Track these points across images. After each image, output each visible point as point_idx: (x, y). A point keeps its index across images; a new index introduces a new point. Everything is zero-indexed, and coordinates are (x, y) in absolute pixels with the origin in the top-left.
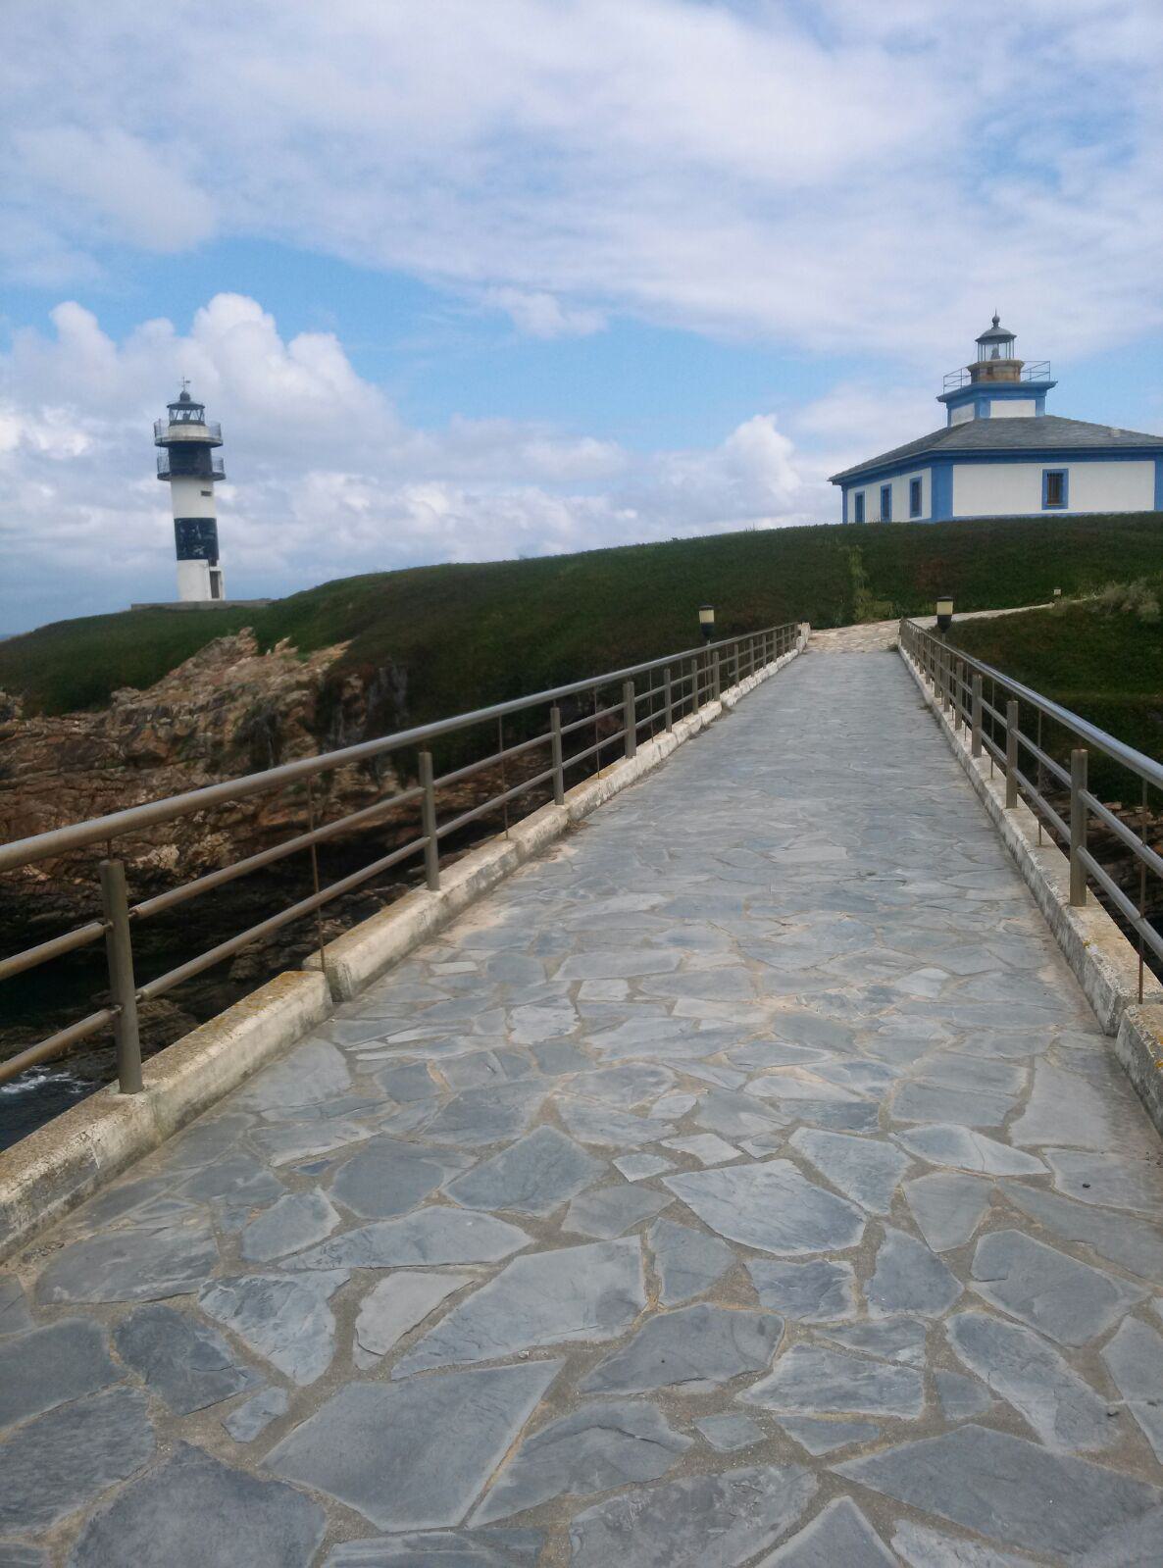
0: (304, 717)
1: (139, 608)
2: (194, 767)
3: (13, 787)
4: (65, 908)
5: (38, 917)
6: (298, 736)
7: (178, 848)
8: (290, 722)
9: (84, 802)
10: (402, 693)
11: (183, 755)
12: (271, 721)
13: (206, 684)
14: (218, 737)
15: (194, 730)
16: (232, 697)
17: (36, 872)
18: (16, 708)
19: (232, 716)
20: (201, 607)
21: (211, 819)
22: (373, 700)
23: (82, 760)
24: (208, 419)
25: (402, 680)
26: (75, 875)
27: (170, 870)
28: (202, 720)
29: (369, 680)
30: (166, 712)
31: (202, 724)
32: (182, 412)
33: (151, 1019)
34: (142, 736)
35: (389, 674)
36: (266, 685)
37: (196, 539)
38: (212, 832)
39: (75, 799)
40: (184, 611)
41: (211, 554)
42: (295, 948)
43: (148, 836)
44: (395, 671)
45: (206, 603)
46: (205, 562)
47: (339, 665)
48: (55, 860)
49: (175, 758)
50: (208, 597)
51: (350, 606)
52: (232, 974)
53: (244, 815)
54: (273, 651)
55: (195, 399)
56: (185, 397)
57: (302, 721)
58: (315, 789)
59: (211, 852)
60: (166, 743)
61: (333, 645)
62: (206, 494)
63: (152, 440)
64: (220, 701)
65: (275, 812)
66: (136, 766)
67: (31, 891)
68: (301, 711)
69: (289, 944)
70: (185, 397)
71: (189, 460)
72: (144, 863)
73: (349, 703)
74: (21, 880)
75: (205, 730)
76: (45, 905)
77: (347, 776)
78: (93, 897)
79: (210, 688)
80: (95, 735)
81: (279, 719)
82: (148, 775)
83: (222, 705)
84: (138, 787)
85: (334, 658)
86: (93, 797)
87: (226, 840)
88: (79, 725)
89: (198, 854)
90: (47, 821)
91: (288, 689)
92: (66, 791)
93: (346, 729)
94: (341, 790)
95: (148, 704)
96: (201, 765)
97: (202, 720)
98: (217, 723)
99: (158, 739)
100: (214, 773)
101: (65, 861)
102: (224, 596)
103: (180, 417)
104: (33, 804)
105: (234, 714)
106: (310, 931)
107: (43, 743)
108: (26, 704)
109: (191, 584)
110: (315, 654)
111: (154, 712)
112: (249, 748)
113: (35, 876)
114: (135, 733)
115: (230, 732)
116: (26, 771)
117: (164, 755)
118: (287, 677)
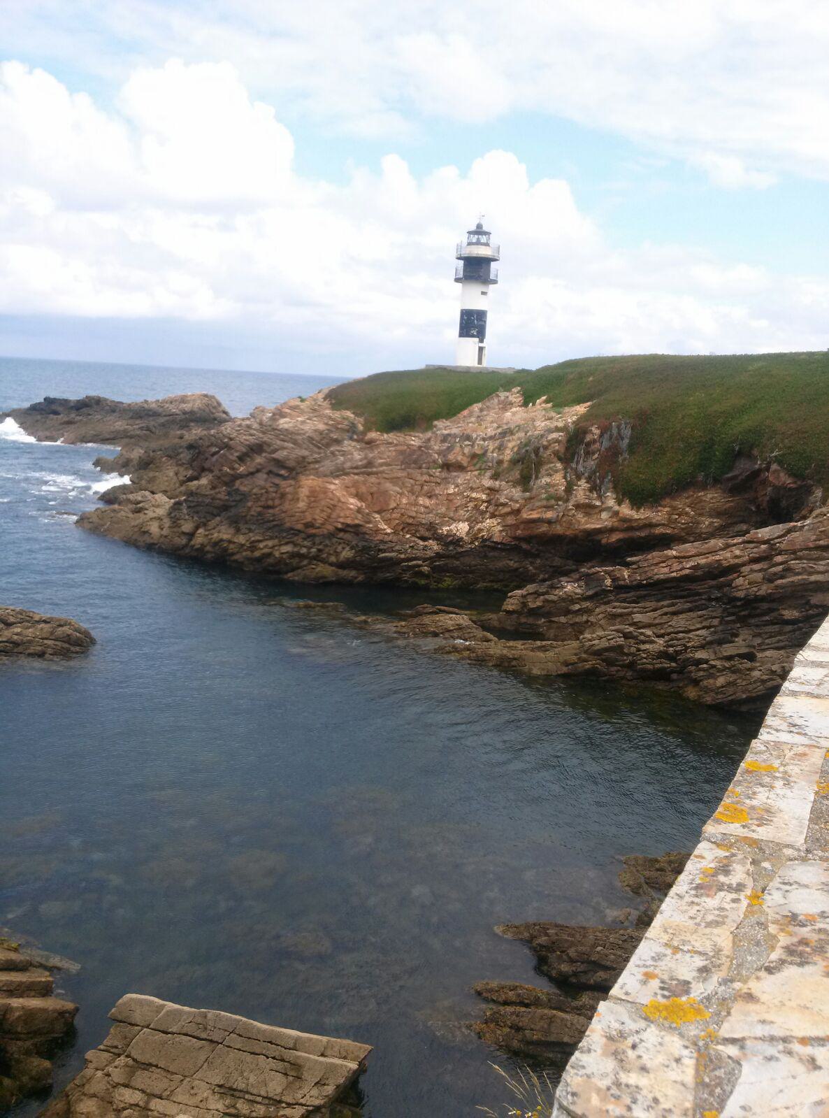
0: (558, 451)
1: (431, 368)
2: (484, 475)
3: (376, 473)
4: (399, 552)
5: (383, 555)
6: (552, 463)
8: (548, 452)
9: (417, 488)
10: (626, 441)
11: (478, 466)
12: (537, 451)
13: (492, 422)
14: (501, 457)
15: (486, 451)
16: (511, 432)
17: (386, 527)
18: (360, 425)
19: (510, 445)
20: (472, 370)
21: (491, 509)
22: (606, 444)
23: (415, 462)
24: (494, 240)
25: (627, 432)
26: (407, 533)
28: (491, 446)
29: (604, 430)
30: (468, 438)
31: (491, 448)
32: (476, 236)
33: (457, 625)
34: (455, 451)
35: (618, 427)
36: (534, 427)
37: (472, 324)
38: (491, 518)
39: (412, 485)
40: (460, 372)
41: (481, 335)
42: (546, 597)
43: (452, 515)
44: (623, 426)
45: (473, 367)
46: (477, 340)
47: (583, 418)
48: (397, 521)
49: (472, 468)
51: (591, 379)
52: (504, 607)
54: (534, 405)
55: (485, 228)
56: (479, 226)
57: (556, 454)
58: (558, 499)
59: (488, 531)
60: (468, 457)
61: (579, 404)
62: (483, 293)
63: (455, 255)
64: (504, 434)
65: (532, 510)
66: (448, 469)
67: (381, 538)
68: (556, 446)
69: (543, 594)
70: (479, 226)
71: (476, 269)
72: (448, 531)
73: (588, 444)
75: (492, 452)
76: (388, 548)
77: (582, 493)
78: (415, 547)
79: (495, 425)
80: (425, 447)
81: (541, 450)
82: (456, 476)
83: (503, 437)
84: (449, 483)
85: (580, 413)
86: (422, 486)
87: (498, 524)
88: (414, 440)
89: (480, 530)
91: (550, 431)
92: (407, 480)
93: (584, 461)
94: (576, 501)
95: (455, 431)
96: (488, 474)
97: (491, 446)
98: (500, 448)
99: (464, 454)
100: (496, 479)
101: (403, 523)
102: (485, 364)
103: (474, 240)
104: (388, 485)
105: (512, 444)
106: (558, 588)
107: (393, 449)
108: (366, 423)
109: (464, 354)
110: (567, 409)
111: (461, 437)
112: (519, 466)
113: (385, 530)
114: (450, 449)
115: (508, 455)
116: (381, 465)
117: (465, 464)
118: (548, 423)
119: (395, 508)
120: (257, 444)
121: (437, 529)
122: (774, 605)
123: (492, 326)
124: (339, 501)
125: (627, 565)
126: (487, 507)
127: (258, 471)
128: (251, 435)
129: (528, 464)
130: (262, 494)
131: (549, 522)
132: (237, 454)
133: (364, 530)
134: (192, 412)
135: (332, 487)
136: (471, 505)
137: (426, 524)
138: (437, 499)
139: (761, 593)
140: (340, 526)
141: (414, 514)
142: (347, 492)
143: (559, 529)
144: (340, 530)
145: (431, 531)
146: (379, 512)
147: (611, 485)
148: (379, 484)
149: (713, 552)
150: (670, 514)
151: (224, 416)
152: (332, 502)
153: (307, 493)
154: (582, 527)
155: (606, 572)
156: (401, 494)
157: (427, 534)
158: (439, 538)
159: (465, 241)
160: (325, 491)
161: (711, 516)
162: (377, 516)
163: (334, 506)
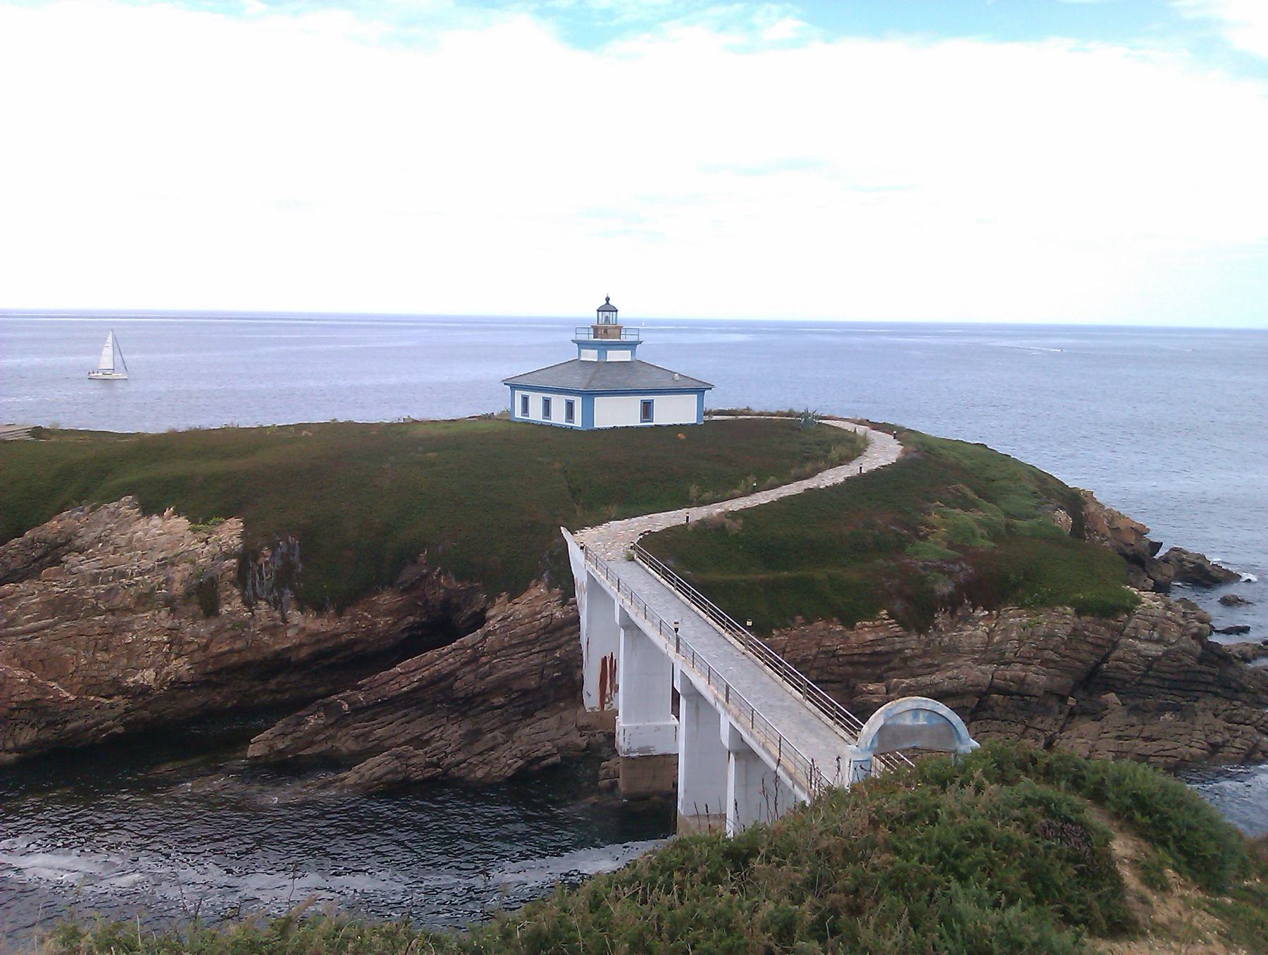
43: (134, 665)
49: (142, 609)
105: (180, 573)
122: (486, 697)
125: (359, 688)
126: (170, 649)
129: (204, 595)
131: (239, 651)
133: (45, 703)
136: (152, 649)
139: (477, 690)
140: (14, 705)
141: (95, 674)
142: (11, 664)
143: (250, 656)
145: (117, 687)
147: (293, 604)
149: (431, 663)
150: (352, 621)
154: (271, 649)
155: (342, 698)
157: (112, 691)
158: (125, 692)
161: (385, 616)
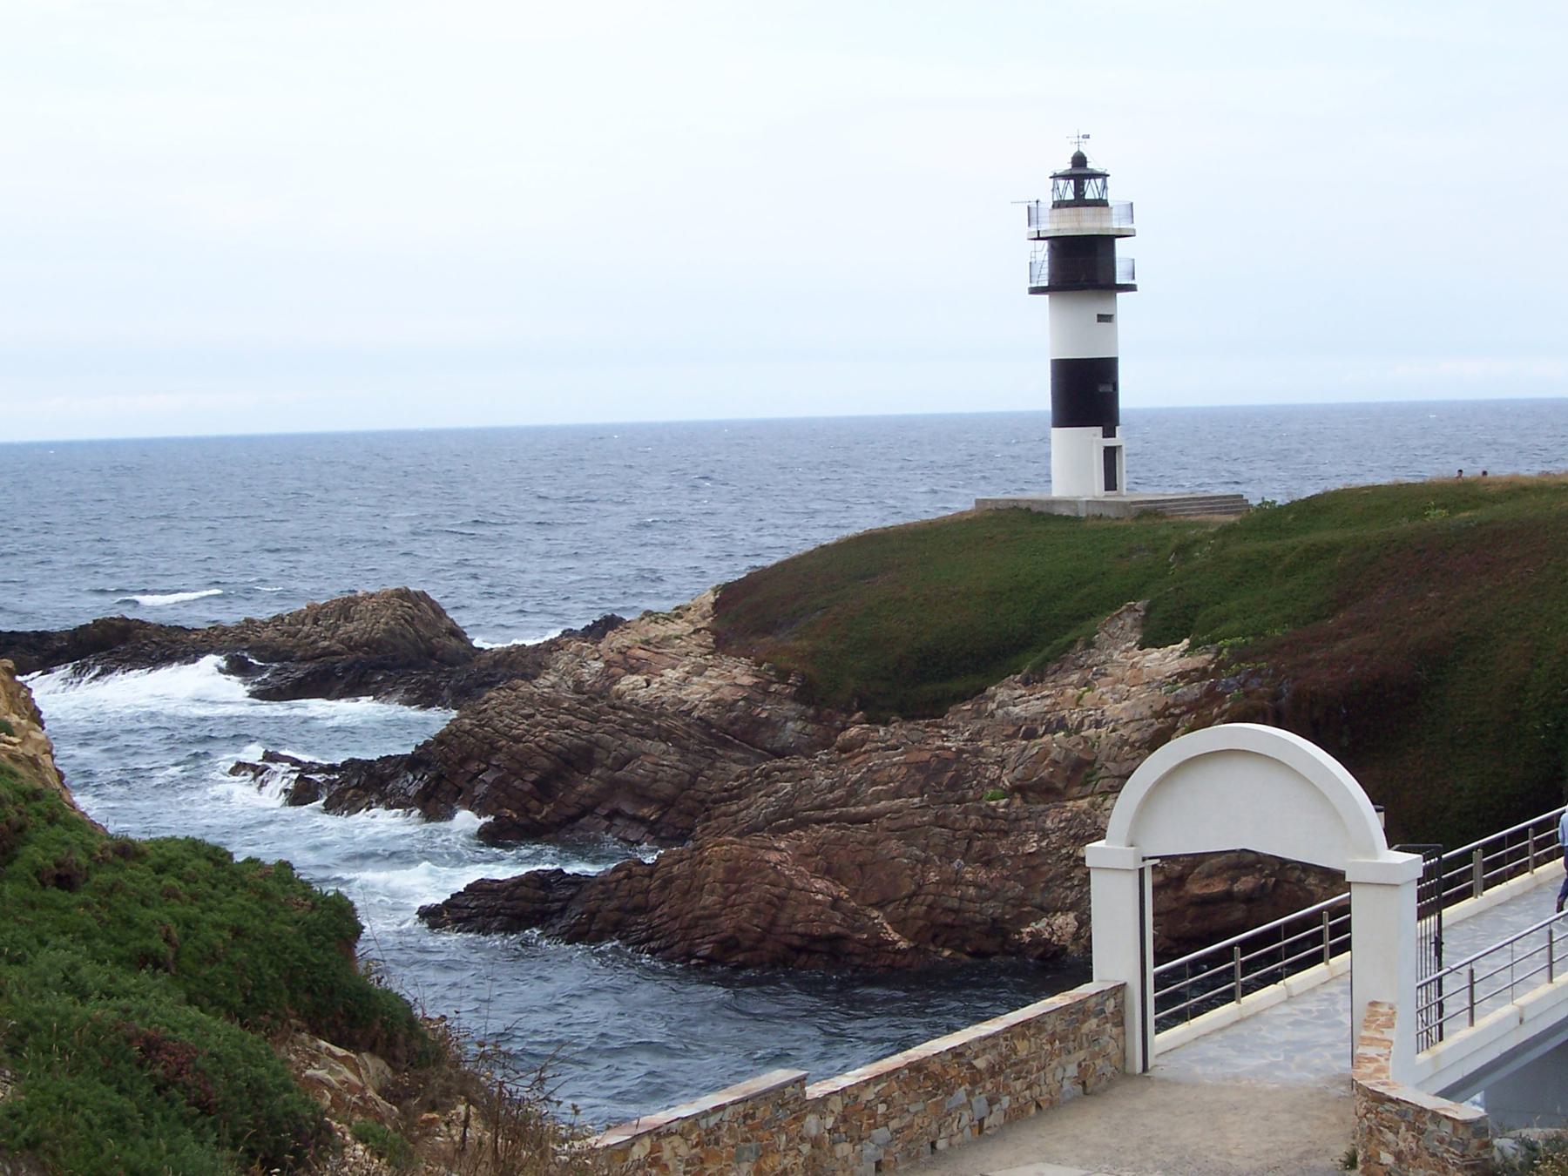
3: (867, 819)
7: (1076, 918)
17: (897, 937)
26: (944, 946)
27: (1064, 948)
37: (1085, 392)
43: (1038, 899)
48: (921, 923)
50: (1097, 489)
53: (1167, 878)
56: (1079, 160)
70: (1079, 160)
72: (1031, 934)
74: (878, 945)
90: (912, 869)
102: (1131, 490)
109: (1068, 469)
113: (895, 942)
117: (1060, 785)
119: (915, 894)
120: (578, 747)
121: (1009, 933)
123: (1131, 394)
124: (791, 887)
127: (586, 811)
128: (562, 726)
130: (618, 881)
132: (532, 777)
134: (372, 645)
135: (774, 857)
137: (985, 923)
138: (1004, 866)
140: (796, 941)
141: (956, 904)
142: (807, 865)
144: (799, 950)
146: (879, 906)
148: (874, 843)
151: (454, 642)
152: (776, 891)
153: (721, 874)
156: (926, 861)
159: (1048, 200)
160: (759, 867)
162: (875, 914)
163: (782, 898)
